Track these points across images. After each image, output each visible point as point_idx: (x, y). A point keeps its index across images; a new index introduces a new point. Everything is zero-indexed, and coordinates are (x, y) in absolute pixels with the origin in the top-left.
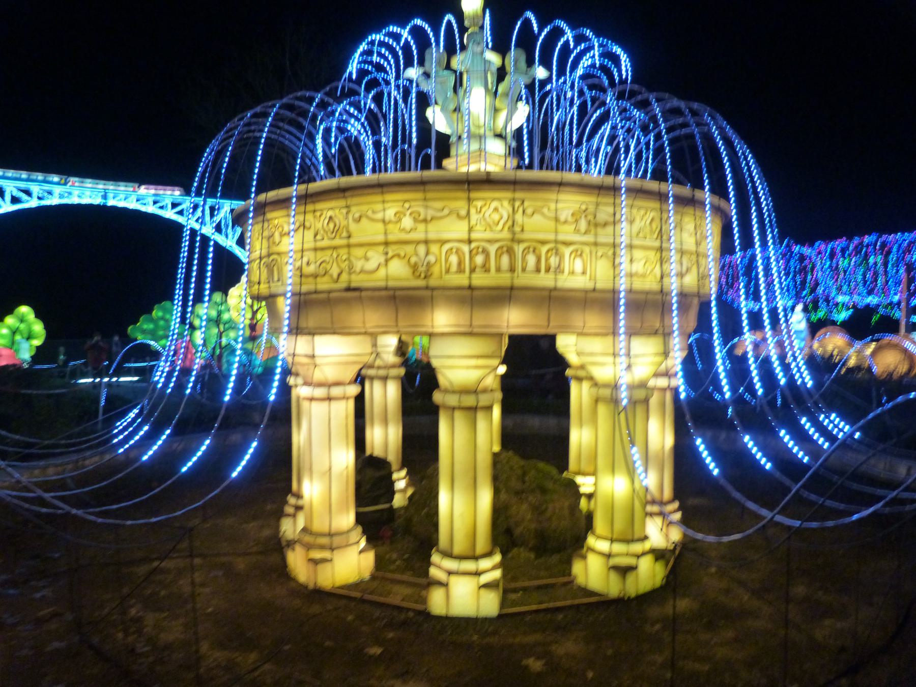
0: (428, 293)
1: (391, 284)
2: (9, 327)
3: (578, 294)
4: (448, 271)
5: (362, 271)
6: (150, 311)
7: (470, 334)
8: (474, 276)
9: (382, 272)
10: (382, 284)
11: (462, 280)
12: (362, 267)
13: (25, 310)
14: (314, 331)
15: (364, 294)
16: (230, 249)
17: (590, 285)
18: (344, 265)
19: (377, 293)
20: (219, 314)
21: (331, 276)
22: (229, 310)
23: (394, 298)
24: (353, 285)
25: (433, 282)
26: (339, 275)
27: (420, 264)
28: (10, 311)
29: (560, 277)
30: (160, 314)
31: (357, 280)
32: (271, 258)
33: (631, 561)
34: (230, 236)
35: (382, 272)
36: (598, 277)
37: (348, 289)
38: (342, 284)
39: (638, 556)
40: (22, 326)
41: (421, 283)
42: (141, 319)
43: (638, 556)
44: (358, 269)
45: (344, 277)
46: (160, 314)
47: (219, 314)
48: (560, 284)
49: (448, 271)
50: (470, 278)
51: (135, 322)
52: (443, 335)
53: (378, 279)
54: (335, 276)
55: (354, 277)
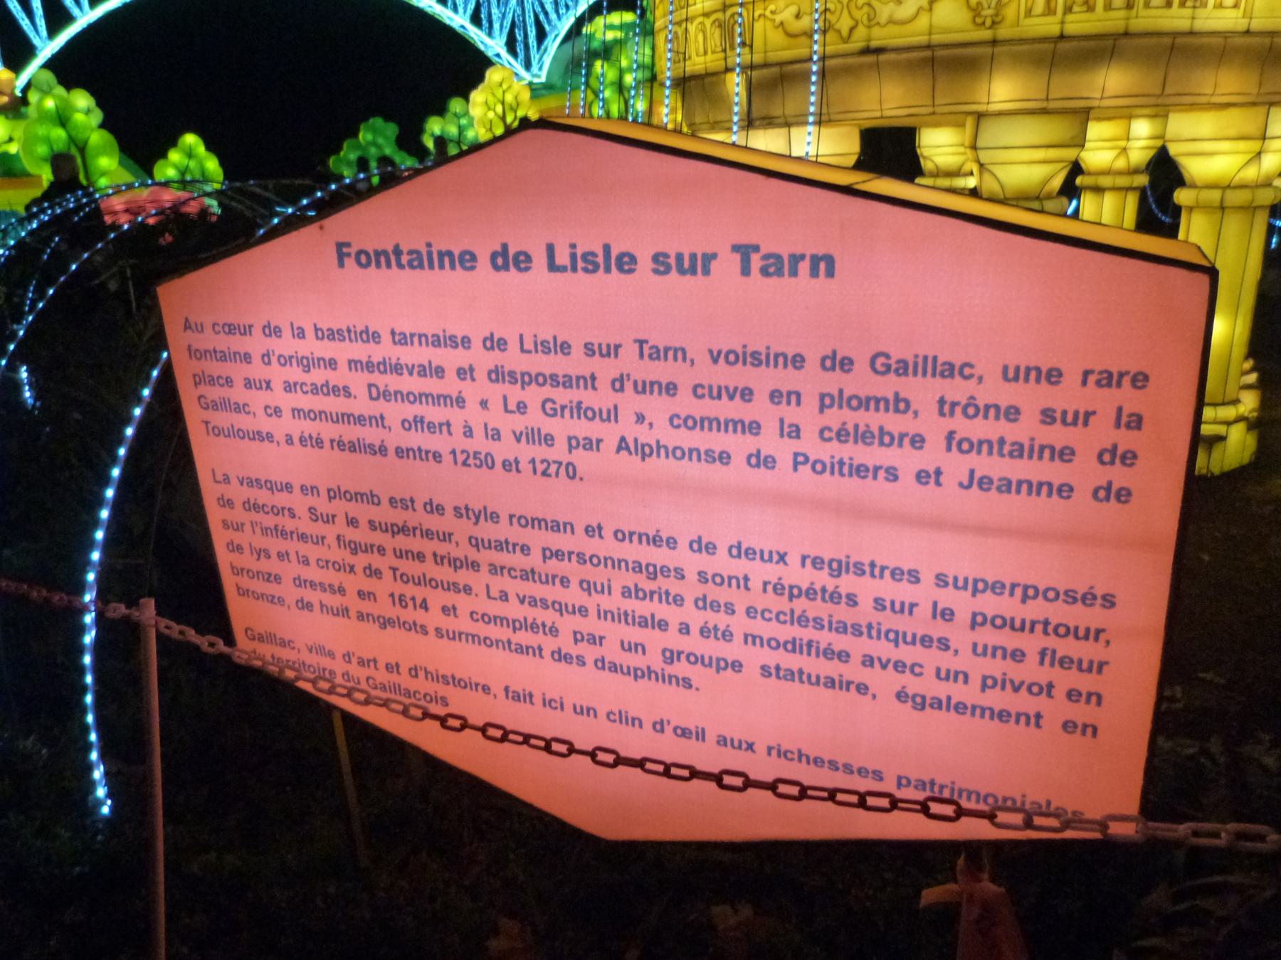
0: (988, 50)
1: (937, 38)
2: (175, 166)
3: (1213, 40)
4: (1029, 13)
5: (891, 21)
6: (355, 134)
7: (1044, 112)
8: (1070, 17)
9: (923, 21)
10: (923, 39)
11: (1050, 26)
12: (891, 16)
13: (190, 139)
14: (794, 120)
15: (883, 57)
16: (460, 31)
17: (1242, 25)
18: (861, 15)
19: (905, 56)
20: (461, 130)
21: (839, 32)
22: (472, 125)
23: (933, 60)
24: (874, 44)
25: (1003, 32)
26: (852, 30)
27: (986, 5)
28: (173, 142)
29: (1201, 12)
30: (369, 137)
31: (880, 37)
32: (729, 13)
33: (1221, 430)
34: (461, 9)
35: (923, 21)
36: (1256, 13)
37: (867, 51)
38: (857, 44)
39: (1228, 424)
40: (192, 164)
41: (986, 34)
42: (345, 145)
43: (1228, 424)
44: (883, 18)
45: (861, 32)
46: (369, 137)
47: (461, 130)
48: (1200, 25)
49: (1029, 13)
50: (1063, 23)
51: (337, 149)
52: (1000, 114)
53: (916, 33)
54: (845, 33)
55: (876, 32)
